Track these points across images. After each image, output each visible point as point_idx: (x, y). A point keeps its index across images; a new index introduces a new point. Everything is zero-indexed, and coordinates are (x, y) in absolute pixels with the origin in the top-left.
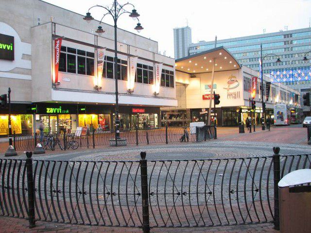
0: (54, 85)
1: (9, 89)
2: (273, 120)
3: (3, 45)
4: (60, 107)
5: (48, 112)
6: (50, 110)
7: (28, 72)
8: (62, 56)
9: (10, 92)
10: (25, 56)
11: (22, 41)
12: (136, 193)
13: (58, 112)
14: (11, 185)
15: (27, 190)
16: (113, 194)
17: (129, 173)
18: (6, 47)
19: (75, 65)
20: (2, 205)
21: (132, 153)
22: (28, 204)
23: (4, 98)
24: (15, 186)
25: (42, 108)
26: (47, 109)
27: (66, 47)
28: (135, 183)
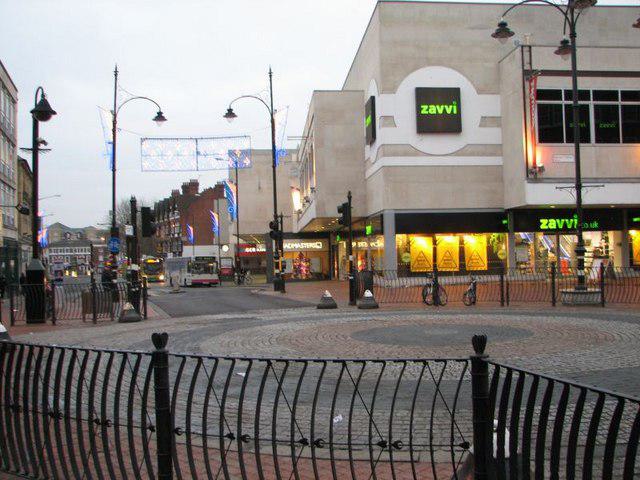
0: (532, 173)
1: (350, 193)
2: (116, 284)
3: (438, 107)
4: (575, 216)
5: (543, 227)
6: (544, 223)
7: (495, 150)
8: (543, 111)
9: (350, 198)
10: (485, 121)
11: (480, 91)
12: (226, 432)
13: (569, 227)
14: (21, 403)
15: (153, 430)
16: (242, 438)
17: (280, 384)
18: (445, 110)
19: (618, 125)
20: (4, 447)
21: (135, 337)
22: (155, 463)
23: (11, 249)
24: (196, 428)
25: (528, 218)
26: (541, 221)
27: (617, 91)
28: (371, 415)
